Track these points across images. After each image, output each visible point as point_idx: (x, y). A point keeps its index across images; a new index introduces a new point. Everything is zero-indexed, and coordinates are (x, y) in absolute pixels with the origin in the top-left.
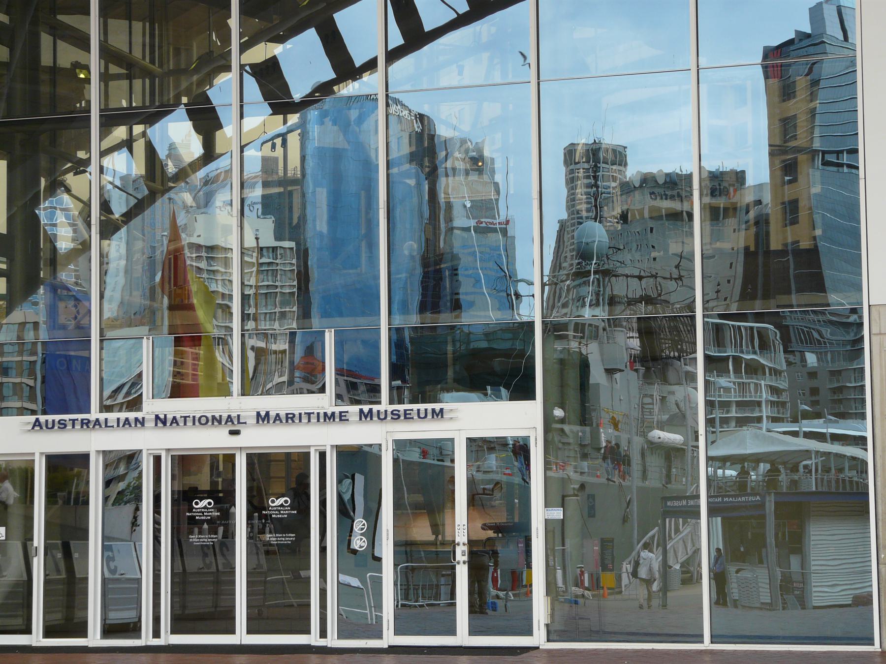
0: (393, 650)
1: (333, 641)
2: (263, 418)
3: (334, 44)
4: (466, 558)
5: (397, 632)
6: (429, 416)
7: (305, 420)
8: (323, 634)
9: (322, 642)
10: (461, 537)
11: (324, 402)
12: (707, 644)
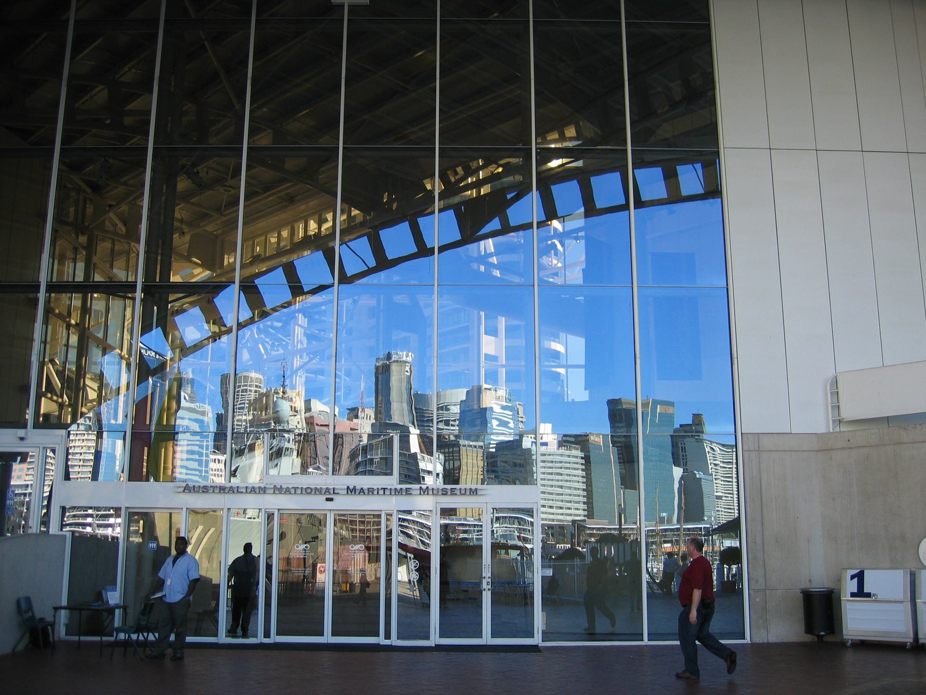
0: (439, 648)
1: (395, 641)
2: (351, 491)
3: (378, 248)
4: (490, 587)
5: (442, 635)
6: (468, 493)
7: (381, 492)
8: (388, 636)
9: (387, 642)
10: (487, 573)
11: (392, 481)
12: (646, 641)
